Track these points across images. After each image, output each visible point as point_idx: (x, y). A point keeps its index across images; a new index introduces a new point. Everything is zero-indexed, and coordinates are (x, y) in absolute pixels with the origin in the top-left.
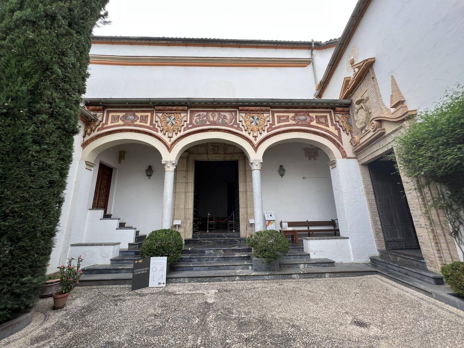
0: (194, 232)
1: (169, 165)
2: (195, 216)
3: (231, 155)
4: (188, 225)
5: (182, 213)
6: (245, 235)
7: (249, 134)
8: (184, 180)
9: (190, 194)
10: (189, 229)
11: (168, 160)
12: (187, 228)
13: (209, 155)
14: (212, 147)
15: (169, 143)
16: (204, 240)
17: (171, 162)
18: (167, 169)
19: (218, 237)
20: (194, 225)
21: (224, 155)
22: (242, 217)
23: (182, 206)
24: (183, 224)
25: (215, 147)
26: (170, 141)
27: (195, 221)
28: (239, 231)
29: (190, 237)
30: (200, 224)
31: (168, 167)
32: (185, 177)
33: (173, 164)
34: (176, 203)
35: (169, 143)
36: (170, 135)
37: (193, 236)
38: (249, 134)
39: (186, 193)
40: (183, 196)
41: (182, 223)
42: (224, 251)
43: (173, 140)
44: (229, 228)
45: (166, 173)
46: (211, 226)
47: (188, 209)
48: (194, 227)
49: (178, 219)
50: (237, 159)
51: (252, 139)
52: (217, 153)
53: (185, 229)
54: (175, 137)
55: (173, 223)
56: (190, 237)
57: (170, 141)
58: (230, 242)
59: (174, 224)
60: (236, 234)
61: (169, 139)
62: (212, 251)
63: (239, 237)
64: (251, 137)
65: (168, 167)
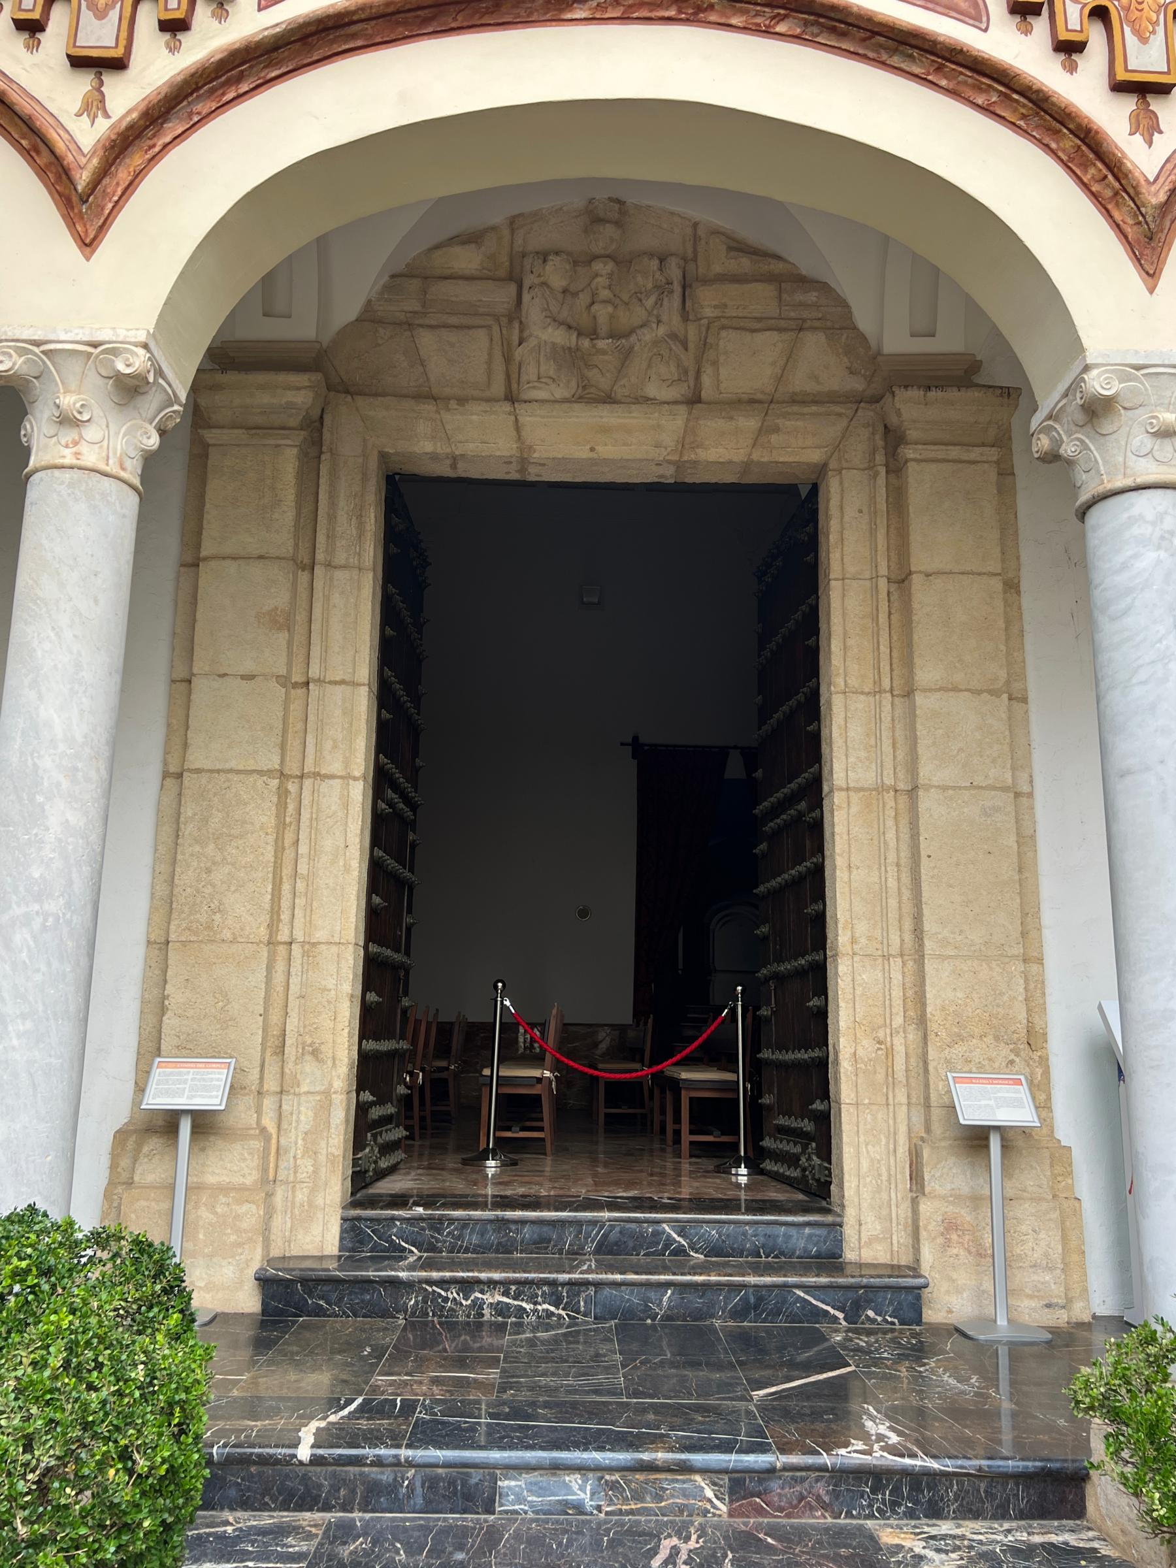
0: (361, 1179)
1: (68, 401)
2: (372, 1022)
3: (749, 423)
4: (303, 1114)
5: (246, 984)
6: (901, 1237)
7: (1069, 48)
8: (272, 655)
9: (331, 793)
10: (311, 1151)
11: (69, 332)
12: (294, 1139)
13: (530, 418)
14: (558, 336)
15: (84, 136)
16: (466, 1286)
17: (96, 351)
18: (45, 444)
19: (612, 1250)
20: (362, 1109)
21: (673, 424)
22: (867, 1047)
23: (245, 912)
24: (245, 1103)
25: (593, 334)
26: (95, 105)
27: (371, 1072)
28: (819, 1191)
29: (316, 1232)
30: (422, 1089)
31: (67, 421)
32: (282, 621)
33: (129, 389)
34: (186, 877)
35: (84, 136)
36: (100, 36)
37: (352, 1232)
38: (1069, 48)
39: (289, 780)
40: (263, 816)
41: (235, 1090)
42: (739, 1486)
43: (126, 96)
44: (686, 1138)
45: (35, 492)
46: (519, 1107)
47: (310, 947)
48: (363, 1127)
49: (195, 1048)
50: (815, 457)
51: (1112, 118)
52: (608, 399)
53: (271, 1152)
54: (156, 67)
55: (140, 1090)
56: (316, 1232)
57: (95, 105)
58: (738, 1314)
59: (159, 1098)
60: (796, 1230)
61: (84, 82)
62: (579, 1489)
63: (919, 1322)
64: (1083, 90)
65: (67, 421)
